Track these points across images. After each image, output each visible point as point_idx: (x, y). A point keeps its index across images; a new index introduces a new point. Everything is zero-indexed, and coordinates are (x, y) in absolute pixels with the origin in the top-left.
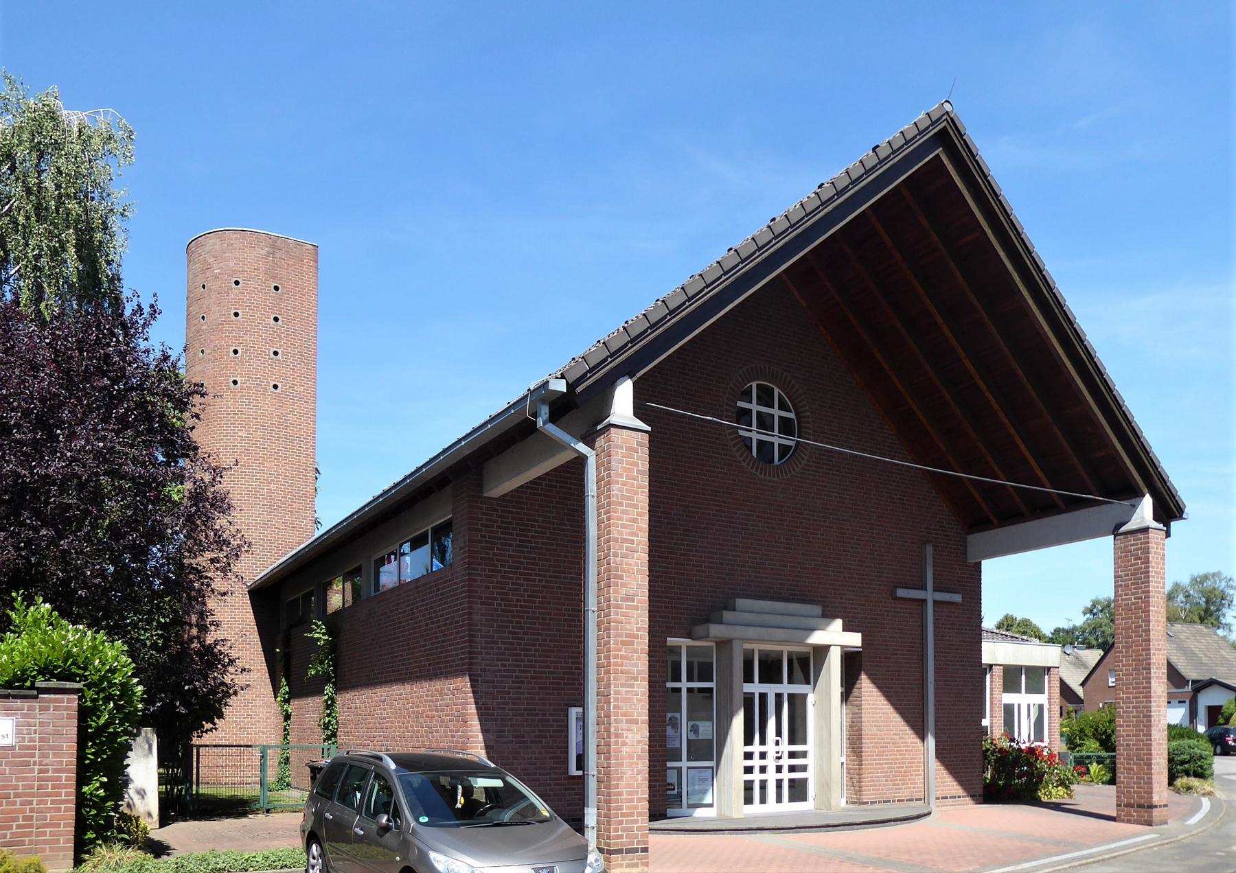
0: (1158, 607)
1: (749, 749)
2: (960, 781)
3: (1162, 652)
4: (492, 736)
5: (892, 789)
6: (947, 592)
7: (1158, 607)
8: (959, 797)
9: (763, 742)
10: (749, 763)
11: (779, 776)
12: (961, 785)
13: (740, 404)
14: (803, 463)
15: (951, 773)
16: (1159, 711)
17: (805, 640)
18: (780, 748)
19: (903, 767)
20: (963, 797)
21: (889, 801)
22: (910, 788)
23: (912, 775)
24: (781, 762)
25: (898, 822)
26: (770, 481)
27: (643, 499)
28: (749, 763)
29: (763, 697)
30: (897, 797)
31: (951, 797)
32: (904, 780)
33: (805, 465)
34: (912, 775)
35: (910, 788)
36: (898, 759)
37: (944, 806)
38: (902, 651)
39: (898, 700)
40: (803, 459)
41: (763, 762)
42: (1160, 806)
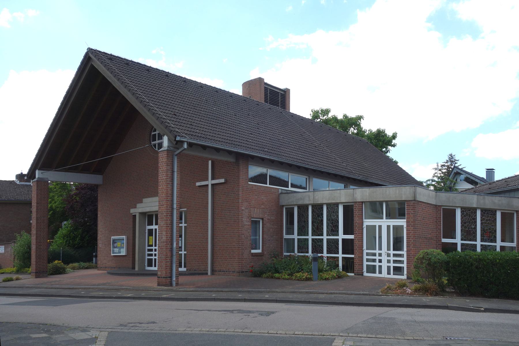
7: (162, 186)
16: (162, 233)
22: (204, 265)
31: (223, 271)
42: (161, 277)
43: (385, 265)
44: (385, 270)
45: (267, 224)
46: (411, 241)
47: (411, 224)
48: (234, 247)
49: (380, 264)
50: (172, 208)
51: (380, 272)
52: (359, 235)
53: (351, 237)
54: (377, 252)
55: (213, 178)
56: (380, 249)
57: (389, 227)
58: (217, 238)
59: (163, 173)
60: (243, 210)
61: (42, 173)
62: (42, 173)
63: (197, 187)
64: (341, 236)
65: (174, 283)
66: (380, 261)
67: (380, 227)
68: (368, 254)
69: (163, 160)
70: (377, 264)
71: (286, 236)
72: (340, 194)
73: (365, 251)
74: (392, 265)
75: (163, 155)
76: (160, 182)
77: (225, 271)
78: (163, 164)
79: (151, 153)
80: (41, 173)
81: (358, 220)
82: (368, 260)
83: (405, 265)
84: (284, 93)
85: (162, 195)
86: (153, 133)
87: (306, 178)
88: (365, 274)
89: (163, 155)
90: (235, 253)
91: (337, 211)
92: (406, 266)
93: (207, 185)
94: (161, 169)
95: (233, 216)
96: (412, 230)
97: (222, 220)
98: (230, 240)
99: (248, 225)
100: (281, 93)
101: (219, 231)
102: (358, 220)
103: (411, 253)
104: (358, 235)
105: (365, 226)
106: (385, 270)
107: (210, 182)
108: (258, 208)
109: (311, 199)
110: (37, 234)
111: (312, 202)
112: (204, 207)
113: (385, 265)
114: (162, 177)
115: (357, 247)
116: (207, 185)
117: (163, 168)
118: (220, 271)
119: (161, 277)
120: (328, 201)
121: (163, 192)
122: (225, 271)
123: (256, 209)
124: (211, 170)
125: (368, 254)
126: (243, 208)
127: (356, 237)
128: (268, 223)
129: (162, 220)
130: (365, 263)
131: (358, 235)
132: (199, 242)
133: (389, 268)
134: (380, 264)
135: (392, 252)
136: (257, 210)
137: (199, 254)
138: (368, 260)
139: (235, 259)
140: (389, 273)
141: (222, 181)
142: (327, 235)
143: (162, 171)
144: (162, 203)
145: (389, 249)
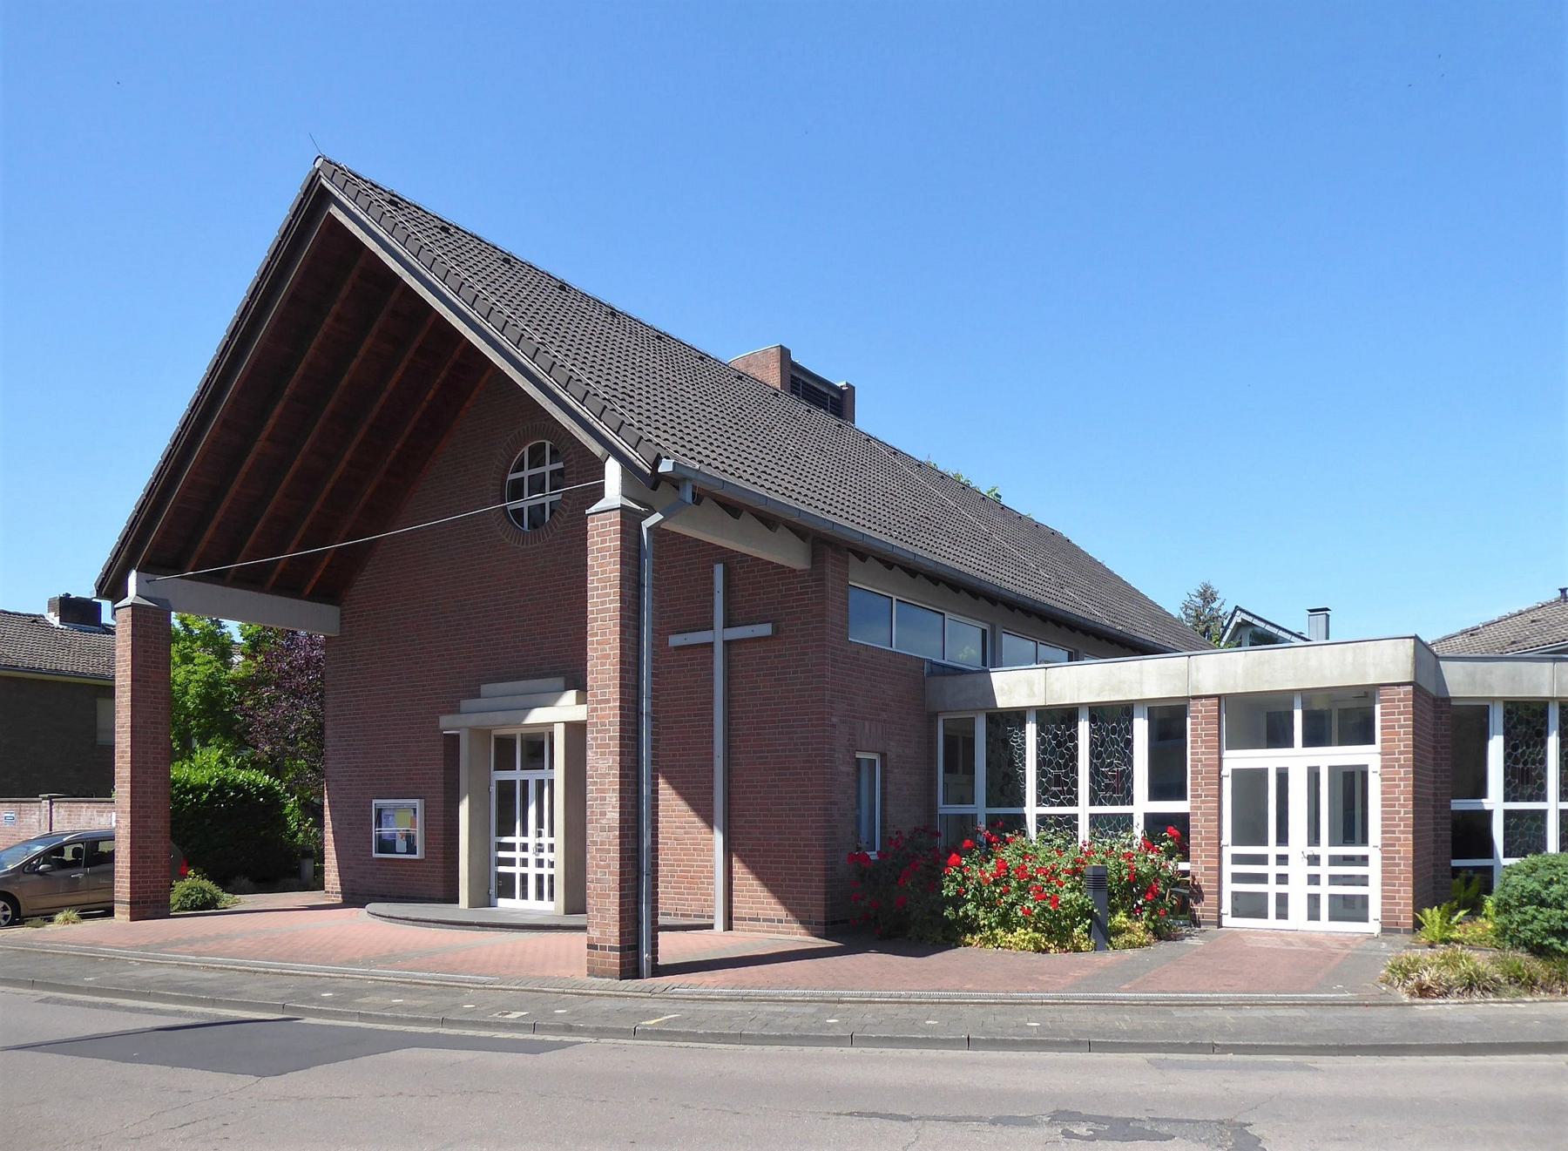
0: (604, 634)
1: (1315, 850)
2: (783, 900)
3: (611, 705)
4: (336, 824)
5: (673, 899)
6: (752, 624)
7: (604, 634)
8: (780, 921)
9: (525, 833)
10: (1282, 869)
11: (540, 871)
12: (784, 904)
13: (560, 465)
14: (568, 508)
15: (766, 885)
16: (604, 799)
17: (523, 720)
18: (541, 840)
19: (690, 872)
20: (787, 922)
21: (670, 915)
22: (699, 900)
23: (703, 883)
24: (541, 856)
25: (488, 928)
26: (533, 549)
27: (129, 654)
28: (1282, 869)
29: (525, 784)
30: (681, 910)
31: (765, 920)
32: (690, 888)
33: (568, 517)
34: (703, 883)
35: (699, 900)
36: (682, 860)
37: (752, 931)
38: (689, 715)
39: (683, 783)
40: (565, 511)
41: (524, 855)
42: (603, 948)
43: (1298, 893)
44: (1297, 907)
45: (896, 771)
46: (1399, 812)
47: (1398, 760)
48: (805, 846)
49: (1282, 889)
50: (639, 713)
51: (1282, 914)
52: (1209, 802)
53: (1459, 805)
54: (1272, 849)
55: (728, 624)
56: (1283, 838)
57: (1314, 774)
58: (744, 816)
59: (605, 588)
60: (833, 726)
61: (148, 582)
62: (148, 582)
63: (670, 649)
64: (1142, 805)
65: (645, 966)
66: (1282, 879)
67: (1283, 776)
68: (1238, 859)
69: (603, 542)
70: (1271, 889)
71: (944, 809)
72: (1141, 672)
73: (1229, 851)
74: (1325, 890)
75: (604, 526)
76: (596, 620)
77: (773, 921)
78: (604, 557)
79: (507, 540)
80: (145, 583)
81: (1203, 753)
82: (1237, 878)
83: (1374, 892)
84: (839, 398)
85: (603, 664)
86: (511, 477)
87: (984, 631)
88: (1228, 921)
89: (604, 526)
90: (811, 863)
91: (1127, 728)
92: (1379, 894)
93: (711, 645)
94: (596, 574)
95: (802, 744)
96: (1400, 779)
97: (761, 757)
98: (790, 822)
99: (848, 774)
100: (832, 397)
101: (751, 793)
102: (1203, 753)
103: (1398, 852)
104: (1202, 802)
105: (1227, 770)
106: (1297, 907)
107: (718, 635)
108: (872, 720)
109: (1036, 692)
110: (331, 815)
111: (1039, 701)
112: (695, 715)
113: (1298, 893)
114: (603, 603)
115: (1202, 839)
116: (711, 645)
117: (604, 572)
118: (759, 920)
119: (603, 948)
120: (1098, 695)
121: (607, 657)
122: (773, 921)
123: (867, 723)
124: (722, 593)
125: (1238, 859)
126: (834, 720)
127: (1199, 808)
128: (898, 768)
129: (603, 754)
130: (1229, 887)
131: (1202, 802)
132: (677, 828)
133: (1314, 900)
134: (1282, 889)
135: (1325, 850)
136: (870, 726)
137: (679, 866)
138: (1237, 878)
139: (811, 881)
140: (1314, 915)
141: (765, 630)
142: (1092, 803)
143: (599, 581)
144: (603, 694)
145: (1314, 839)
